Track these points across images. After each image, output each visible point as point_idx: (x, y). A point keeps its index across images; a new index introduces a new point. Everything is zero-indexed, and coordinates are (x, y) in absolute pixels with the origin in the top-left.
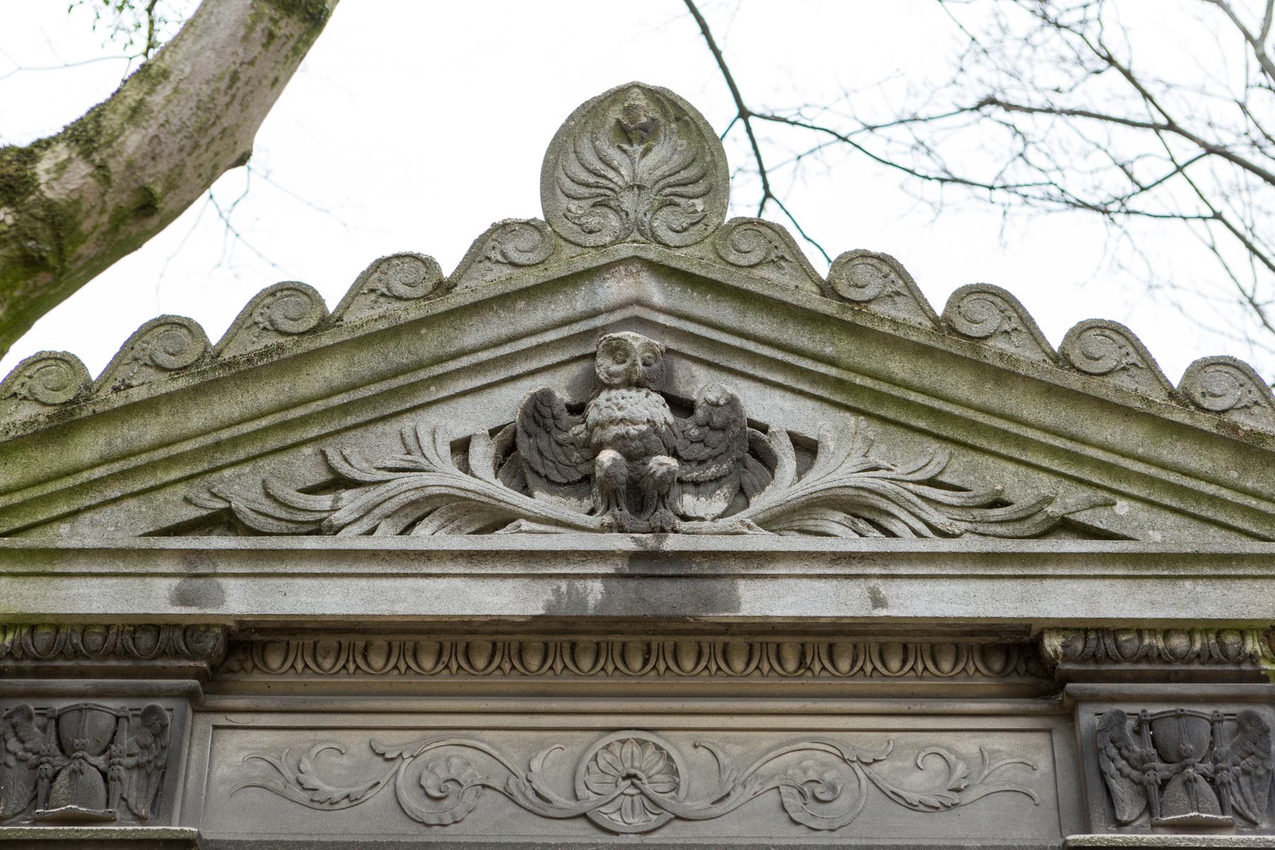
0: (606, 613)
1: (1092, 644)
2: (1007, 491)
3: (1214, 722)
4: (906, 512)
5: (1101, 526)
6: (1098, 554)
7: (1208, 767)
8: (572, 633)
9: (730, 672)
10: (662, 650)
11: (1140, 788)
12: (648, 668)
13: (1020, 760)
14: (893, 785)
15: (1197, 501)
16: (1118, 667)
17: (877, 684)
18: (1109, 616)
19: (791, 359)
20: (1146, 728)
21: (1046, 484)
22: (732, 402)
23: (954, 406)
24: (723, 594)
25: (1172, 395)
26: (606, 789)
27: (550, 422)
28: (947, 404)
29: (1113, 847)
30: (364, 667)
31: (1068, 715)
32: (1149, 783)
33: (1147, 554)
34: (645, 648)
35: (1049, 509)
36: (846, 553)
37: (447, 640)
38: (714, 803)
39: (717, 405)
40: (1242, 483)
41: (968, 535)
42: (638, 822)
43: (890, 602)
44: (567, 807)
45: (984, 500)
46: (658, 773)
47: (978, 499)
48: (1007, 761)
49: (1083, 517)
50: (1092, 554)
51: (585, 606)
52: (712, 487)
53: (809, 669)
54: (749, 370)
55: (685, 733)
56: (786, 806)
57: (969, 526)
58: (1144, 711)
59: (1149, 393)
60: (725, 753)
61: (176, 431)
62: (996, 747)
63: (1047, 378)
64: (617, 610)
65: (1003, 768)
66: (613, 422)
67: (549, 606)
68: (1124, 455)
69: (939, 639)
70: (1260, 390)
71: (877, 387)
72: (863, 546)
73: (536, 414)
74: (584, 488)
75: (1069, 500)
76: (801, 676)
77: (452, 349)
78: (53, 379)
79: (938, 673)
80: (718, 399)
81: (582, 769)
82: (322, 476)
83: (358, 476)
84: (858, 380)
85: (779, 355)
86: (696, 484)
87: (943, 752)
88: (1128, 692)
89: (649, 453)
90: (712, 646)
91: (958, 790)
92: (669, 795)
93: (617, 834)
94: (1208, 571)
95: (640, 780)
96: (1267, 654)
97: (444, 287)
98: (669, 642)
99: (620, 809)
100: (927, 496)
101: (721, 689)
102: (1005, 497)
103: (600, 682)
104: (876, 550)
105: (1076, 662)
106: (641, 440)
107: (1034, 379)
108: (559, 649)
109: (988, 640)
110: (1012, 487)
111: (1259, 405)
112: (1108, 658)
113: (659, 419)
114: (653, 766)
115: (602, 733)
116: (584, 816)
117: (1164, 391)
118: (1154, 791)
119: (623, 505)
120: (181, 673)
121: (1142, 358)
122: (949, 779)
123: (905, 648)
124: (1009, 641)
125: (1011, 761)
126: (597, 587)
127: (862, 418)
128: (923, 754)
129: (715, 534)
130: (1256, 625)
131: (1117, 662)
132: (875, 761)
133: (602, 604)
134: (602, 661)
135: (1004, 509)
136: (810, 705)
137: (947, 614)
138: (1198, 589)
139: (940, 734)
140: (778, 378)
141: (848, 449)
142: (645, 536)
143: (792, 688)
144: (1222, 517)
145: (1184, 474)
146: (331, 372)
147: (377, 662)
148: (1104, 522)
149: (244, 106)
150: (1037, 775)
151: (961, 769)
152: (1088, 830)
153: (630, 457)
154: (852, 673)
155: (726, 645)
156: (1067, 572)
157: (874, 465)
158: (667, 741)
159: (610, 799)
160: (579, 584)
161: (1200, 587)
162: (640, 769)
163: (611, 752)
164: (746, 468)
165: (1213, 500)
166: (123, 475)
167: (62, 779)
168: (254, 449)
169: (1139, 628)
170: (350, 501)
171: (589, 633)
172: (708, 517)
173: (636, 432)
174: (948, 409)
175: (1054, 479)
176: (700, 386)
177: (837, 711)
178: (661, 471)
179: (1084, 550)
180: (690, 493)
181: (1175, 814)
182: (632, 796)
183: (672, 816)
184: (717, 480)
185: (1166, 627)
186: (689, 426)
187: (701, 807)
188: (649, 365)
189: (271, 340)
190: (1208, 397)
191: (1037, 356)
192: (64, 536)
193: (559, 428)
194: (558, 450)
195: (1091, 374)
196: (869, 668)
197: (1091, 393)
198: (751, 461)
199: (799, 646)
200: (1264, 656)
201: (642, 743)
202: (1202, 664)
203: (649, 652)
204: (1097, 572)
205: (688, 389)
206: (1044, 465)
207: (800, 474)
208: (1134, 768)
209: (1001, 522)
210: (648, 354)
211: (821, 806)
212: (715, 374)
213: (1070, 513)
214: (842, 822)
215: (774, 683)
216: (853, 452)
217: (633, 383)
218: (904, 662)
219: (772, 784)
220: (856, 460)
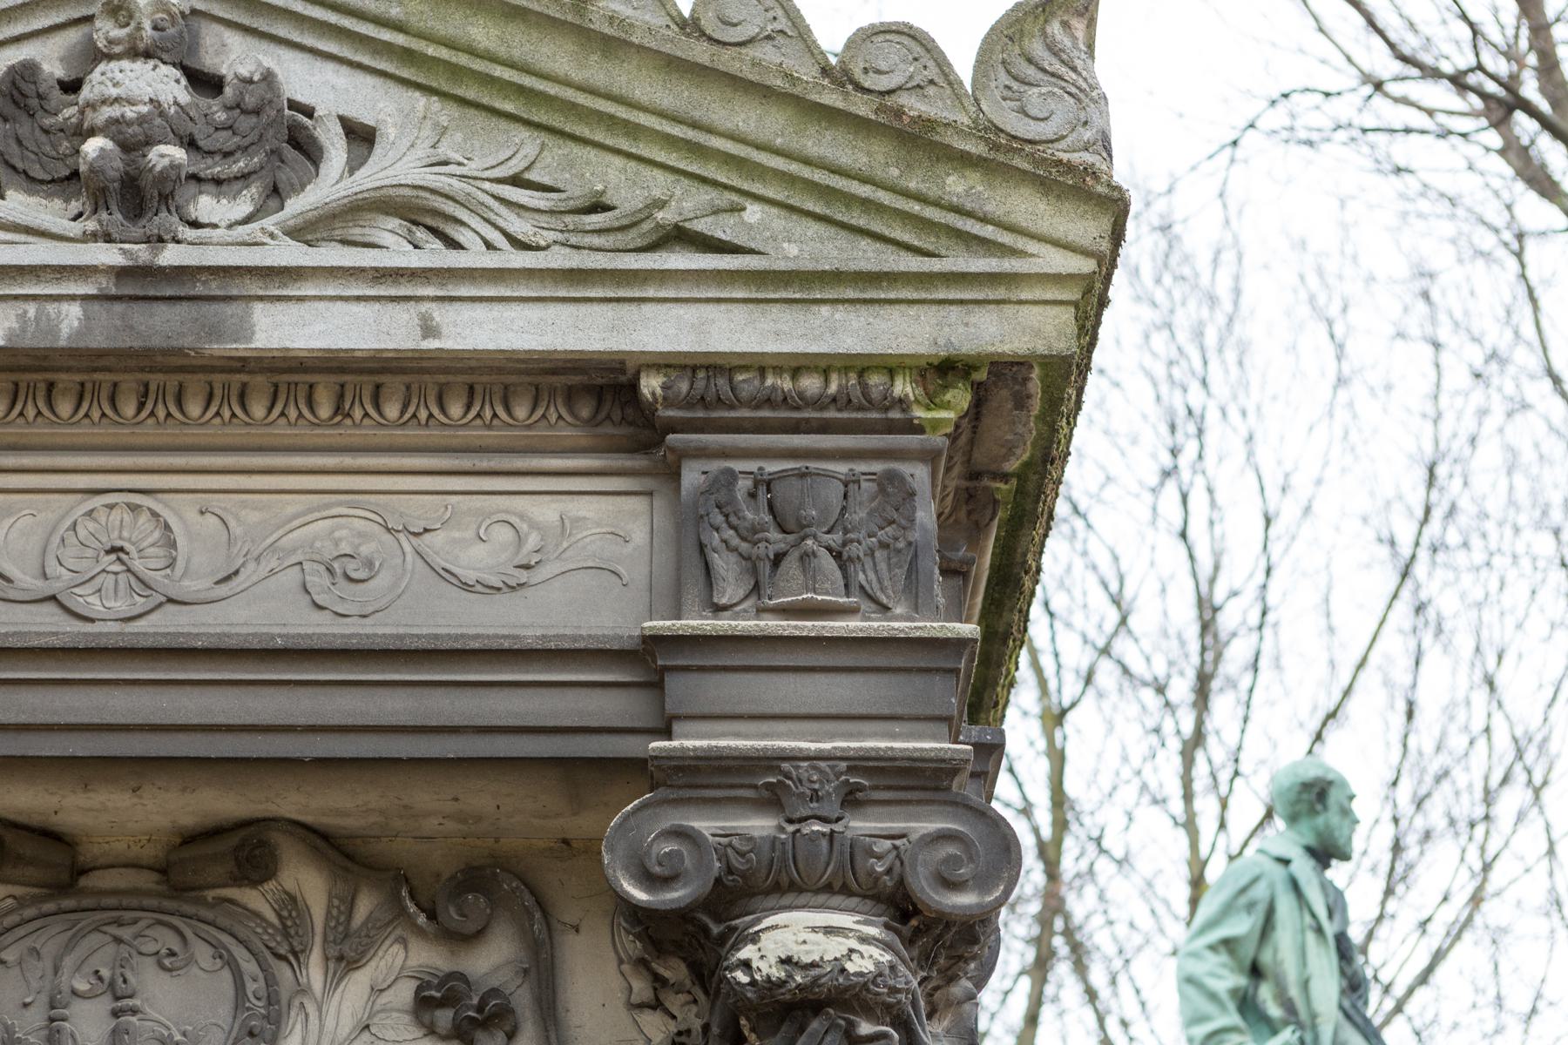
0: (82, 345)
1: (700, 384)
2: (610, 193)
4: (478, 219)
5: (723, 237)
6: (711, 271)
7: (835, 539)
8: (46, 370)
9: (247, 419)
10: (162, 392)
11: (749, 564)
12: (144, 414)
13: (609, 530)
14: (447, 561)
15: (848, 206)
16: (733, 414)
17: (434, 435)
18: (721, 349)
20: (762, 490)
21: (659, 184)
22: (268, 77)
23: (550, 84)
24: (233, 321)
25: (826, 71)
26: (85, 564)
27: (34, 102)
28: (540, 81)
29: (700, 636)
30: (177, 415)
31: (673, 475)
32: (758, 557)
33: (775, 272)
34: (142, 389)
35: (660, 215)
36: (392, 269)
38: (217, 583)
39: (250, 81)
40: (903, 183)
41: (556, 248)
42: (121, 606)
43: (445, 330)
44: (33, 587)
45: (579, 203)
46: (153, 545)
47: (572, 202)
48: (594, 531)
49: (701, 226)
50: (704, 271)
51: (56, 336)
52: (237, 185)
53: (348, 415)
54: (296, 37)
55: (191, 496)
56: (308, 586)
57: (560, 237)
58: (760, 469)
59: (797, 67)
60: (238, 520)
62: (582, 513)
63: (667, 48)
64: (98, 341)
65: (588, 540)
66: (104, 102)
68: (759, 147)
69: (513, 379)
70: (939, 65)
71: (454, 60)
72: (415, 260)
73: (15, 93)
74: (73, 186)
76: (338, 424)
79: (511, 421)
80: (252, 74)
81: (56, 540)
84: (431, 51)
86: (218, 182)
87: (513, 519)
88: (743, 445)
89: (149, 142)
90: (226, 387)
91: (527, 567)
92: (163, 572)
93: (92, 620)
94: (851, 294)
95: (127, 554)
96: (920, 398)
98: (172, 381)
99: (100, 590)
100: (508, 197)
101: (237, 441)
102: (607, 200)
103: (83, 433)
104: (430, 265)
105: (680, 408)
106: (140, 125)
107: (650, 49)
108: (31, 390)
109: (575, 379)
110: (617, 188)
111: (935, 84)
112: (720, 402)
114: (146, 537)
115: (86, 496)
116: (53, 598)
117: (817, 66)
118: (765, 568)
119: (114, 208)
121: (793, 23)
122: (517, 552)
123: (471, 389)
124: (599, 381)
125: (598, 530)
126: (74, 311)
127: (435, 98)
128: (489, 522)
129: (228, 244)
130: (908, 362)
131: (732, 407)
132: (426, 530)
133: (79, 333)
134: (85, 406)
135: (604, 215)
136: (348, 461)
137: (515, 347)
138: (837, 316)
139: (513, 497)
141: (413, 138)
142: (136, 247)
143: (327, 440)
144: (877, 226)
145: (833, 172)
148: (728, 231)
150: (630, 547)
151: (533, 541)
153: (126, 147)
154: (402, 421)
155: (244, 385)
156: (672, 294)
157: (443, 158)
158: (166, 505)
159: (87, 577)
160: (51, 308)
161: (840, 313)
162: (129, 540)
163: (95, 520)
164: (283, 162)
165: (867, 204)
169: (761, 365)
171: (69, 370)
172: (223, 224)
173: (135, 115)
174: (541, 87)
175: (671, 177)
176: (233, 57)
177: (382, 468)
178: (161, 164)
179: (694, 267)
180: (208, 193)
181: (786, 596)
182: (116, 573)
183: (163, 599)
184: (244, 177)
185: (794, 364)
186: (215, 109)
187: (200, 587)
188: (163, 30)
190: (871, 74)
191: (658, 20)
193: (46, 111)
194: (43, 138)
195: (725, 44)
196: (423, 414)
197: (721, 67)
198: (290, 153)
199: (337, 387)
200: (917, 401)
201: (134, 508)
202: (840, 410)
203: (146, 395)
204: (710, 295)
205: (216, 60)
206: (658, 159)
207: (353, 167)
208: (744, 539)
209: (599, 232)
210: (160, 15)
211: (353, 586)
213: (685, 220)
214: (377, 607)
216: (419, 142)
217: (137, 52)
218: (468, 407)
219: (294, 560)
220: (422, 151)
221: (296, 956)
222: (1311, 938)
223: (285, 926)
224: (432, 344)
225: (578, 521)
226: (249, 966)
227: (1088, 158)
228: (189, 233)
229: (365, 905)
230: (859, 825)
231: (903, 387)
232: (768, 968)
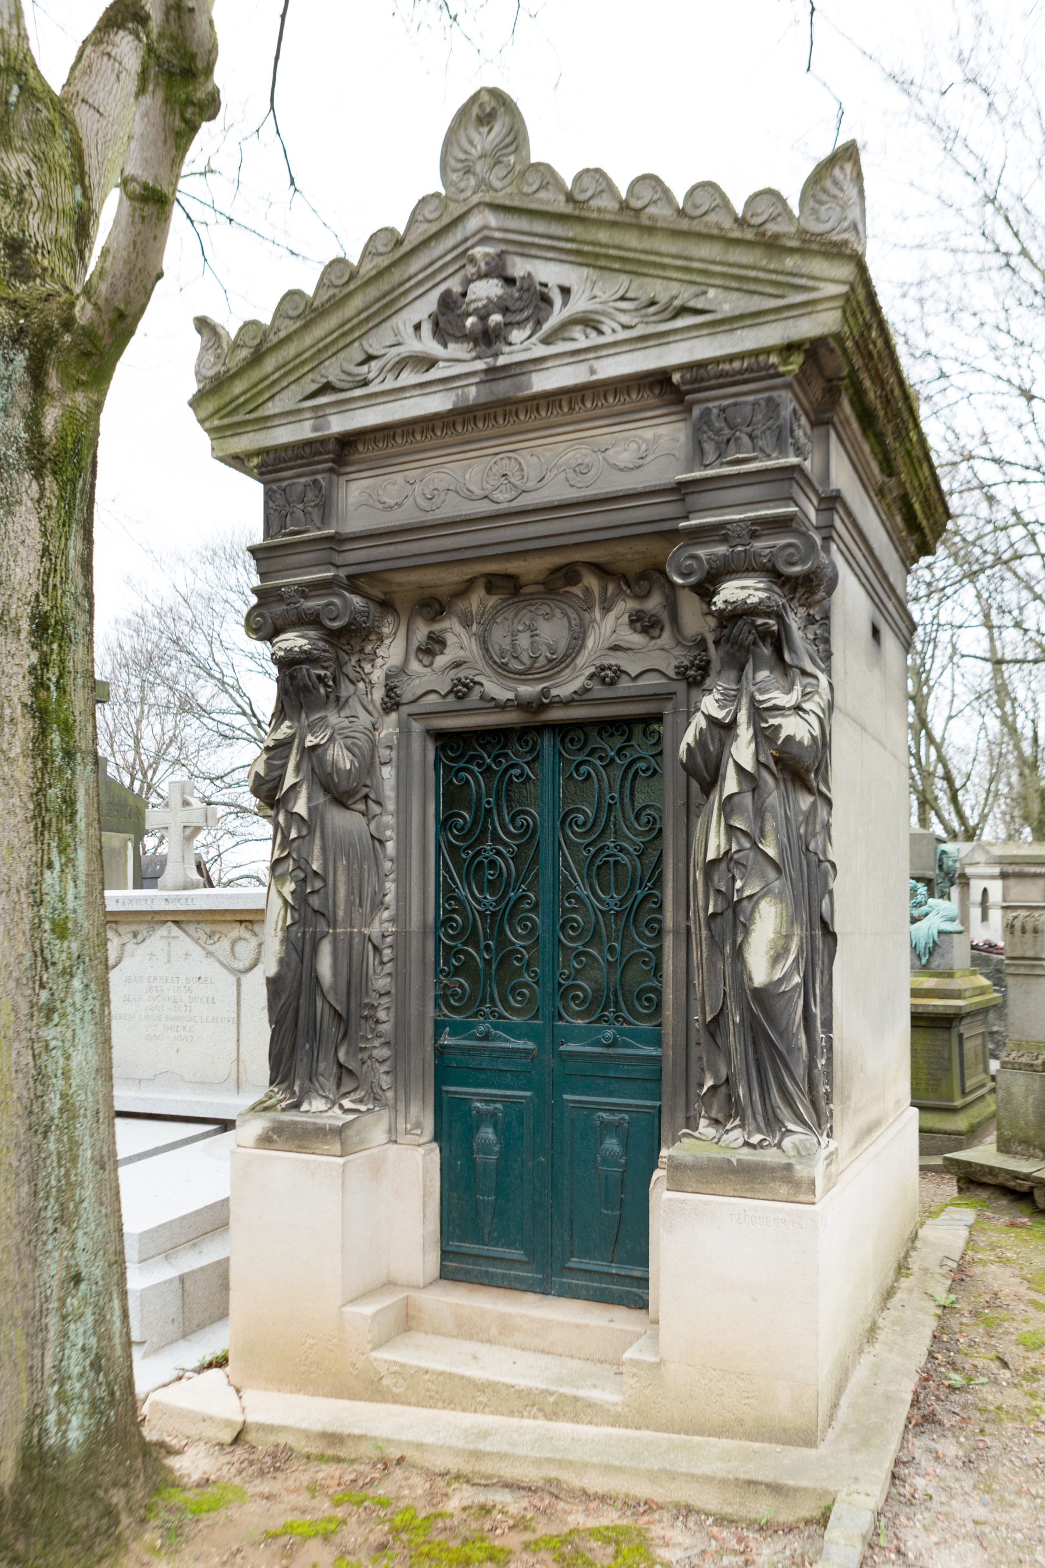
3: (755, 403)
7: (749, 429)
19: (555, 243)
21: (675, 288)
37: (424, 425)
42: (508, 496)
49: (692, 304)
61: (301, 348)
63: (671, 226)
64: (482, 400)
67: (454, 403)
75: (685, 295)
77: (406, 277)
78: (251, 334)
82: (361, 357)
85: (549, 242)
89: (488, 315)
97: (399, 242)
98: (514, 407)
112: (702, 380)
133: (476, 398)
140: (551, 255)
146: (357, 302)
147: (399, 440)
149: (145, 255)
165: (756, 280)
166: (286, 374)
168: (334, 349)
169: (717, 361)
170: (375, 365)
184: (527, 319)
189: (331, 292)
192: (271, 409)
198: (543, 305)
201: (509, 458)
207: (565, 303)
215: (561, 419)
220: (587, 294)
223: (171, 741)
224: (594, 378)
225: (660, 436)
226: (573, 615)
227: (845, 236)
229: (611, 589)
230: (758, 544)
231: (773, 359)
232: (720, 605)
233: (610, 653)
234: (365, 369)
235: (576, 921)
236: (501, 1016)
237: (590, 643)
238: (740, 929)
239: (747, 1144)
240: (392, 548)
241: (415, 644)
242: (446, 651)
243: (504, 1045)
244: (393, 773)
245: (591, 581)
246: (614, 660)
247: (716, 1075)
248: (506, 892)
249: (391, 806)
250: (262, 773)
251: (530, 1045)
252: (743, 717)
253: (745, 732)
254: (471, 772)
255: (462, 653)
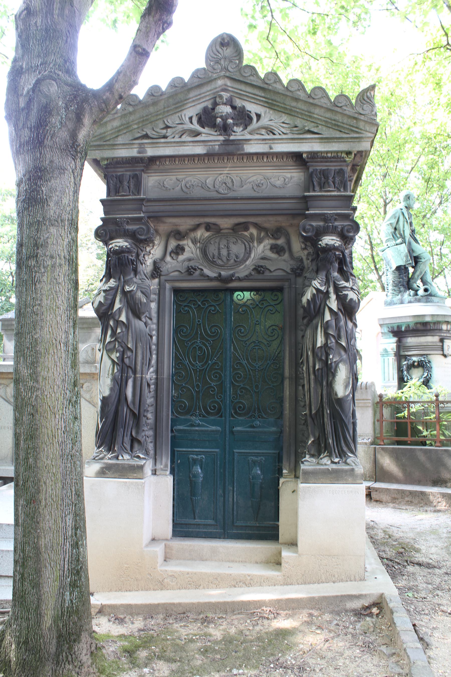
17: (272, 164)
22: (244, 107)
31: (308, 169)
49: (312, 129)
67: (207, 150)
82: (164, 126)
83: (171, 126)
85: (253, 96)
113: (229, 112)
120: (141, 166)
151: (287, 180)
152: (309, 192)
153: (223, 120)
167: (121, 188)
169: (321, 152)
184: (241, 124)
207: (258, 120)
212: (240, 100)
221: (253, 242)
222: (405, 223)
224: (272, 151)
225: (293, 177)
226: (246, 244)
228: (233, 134)
230: (336, 224)
232: (323, 245)
233: (262, 261)
234: (165, 131)
235: (240, 374)
236: (204, 416)
237: (252, 256)
238: (331, 374)
239: (333, 462)
240: (171, 207)
241: (169, 249)
242: (185, 254)
243: (203, 429)
244: (156, 306)
245: (254, 231)
246: (262, 263)
247: (314, 437)
248: (206, 362)
249: (155, 320)
250: (102, 301)
251: (219, 428)
252: (331, 290)
253: (333, 297)
254: (191, 307)
255: (192, 255)
